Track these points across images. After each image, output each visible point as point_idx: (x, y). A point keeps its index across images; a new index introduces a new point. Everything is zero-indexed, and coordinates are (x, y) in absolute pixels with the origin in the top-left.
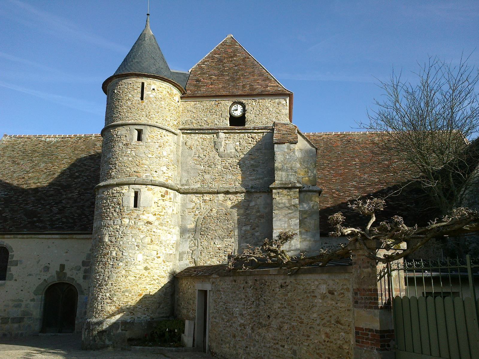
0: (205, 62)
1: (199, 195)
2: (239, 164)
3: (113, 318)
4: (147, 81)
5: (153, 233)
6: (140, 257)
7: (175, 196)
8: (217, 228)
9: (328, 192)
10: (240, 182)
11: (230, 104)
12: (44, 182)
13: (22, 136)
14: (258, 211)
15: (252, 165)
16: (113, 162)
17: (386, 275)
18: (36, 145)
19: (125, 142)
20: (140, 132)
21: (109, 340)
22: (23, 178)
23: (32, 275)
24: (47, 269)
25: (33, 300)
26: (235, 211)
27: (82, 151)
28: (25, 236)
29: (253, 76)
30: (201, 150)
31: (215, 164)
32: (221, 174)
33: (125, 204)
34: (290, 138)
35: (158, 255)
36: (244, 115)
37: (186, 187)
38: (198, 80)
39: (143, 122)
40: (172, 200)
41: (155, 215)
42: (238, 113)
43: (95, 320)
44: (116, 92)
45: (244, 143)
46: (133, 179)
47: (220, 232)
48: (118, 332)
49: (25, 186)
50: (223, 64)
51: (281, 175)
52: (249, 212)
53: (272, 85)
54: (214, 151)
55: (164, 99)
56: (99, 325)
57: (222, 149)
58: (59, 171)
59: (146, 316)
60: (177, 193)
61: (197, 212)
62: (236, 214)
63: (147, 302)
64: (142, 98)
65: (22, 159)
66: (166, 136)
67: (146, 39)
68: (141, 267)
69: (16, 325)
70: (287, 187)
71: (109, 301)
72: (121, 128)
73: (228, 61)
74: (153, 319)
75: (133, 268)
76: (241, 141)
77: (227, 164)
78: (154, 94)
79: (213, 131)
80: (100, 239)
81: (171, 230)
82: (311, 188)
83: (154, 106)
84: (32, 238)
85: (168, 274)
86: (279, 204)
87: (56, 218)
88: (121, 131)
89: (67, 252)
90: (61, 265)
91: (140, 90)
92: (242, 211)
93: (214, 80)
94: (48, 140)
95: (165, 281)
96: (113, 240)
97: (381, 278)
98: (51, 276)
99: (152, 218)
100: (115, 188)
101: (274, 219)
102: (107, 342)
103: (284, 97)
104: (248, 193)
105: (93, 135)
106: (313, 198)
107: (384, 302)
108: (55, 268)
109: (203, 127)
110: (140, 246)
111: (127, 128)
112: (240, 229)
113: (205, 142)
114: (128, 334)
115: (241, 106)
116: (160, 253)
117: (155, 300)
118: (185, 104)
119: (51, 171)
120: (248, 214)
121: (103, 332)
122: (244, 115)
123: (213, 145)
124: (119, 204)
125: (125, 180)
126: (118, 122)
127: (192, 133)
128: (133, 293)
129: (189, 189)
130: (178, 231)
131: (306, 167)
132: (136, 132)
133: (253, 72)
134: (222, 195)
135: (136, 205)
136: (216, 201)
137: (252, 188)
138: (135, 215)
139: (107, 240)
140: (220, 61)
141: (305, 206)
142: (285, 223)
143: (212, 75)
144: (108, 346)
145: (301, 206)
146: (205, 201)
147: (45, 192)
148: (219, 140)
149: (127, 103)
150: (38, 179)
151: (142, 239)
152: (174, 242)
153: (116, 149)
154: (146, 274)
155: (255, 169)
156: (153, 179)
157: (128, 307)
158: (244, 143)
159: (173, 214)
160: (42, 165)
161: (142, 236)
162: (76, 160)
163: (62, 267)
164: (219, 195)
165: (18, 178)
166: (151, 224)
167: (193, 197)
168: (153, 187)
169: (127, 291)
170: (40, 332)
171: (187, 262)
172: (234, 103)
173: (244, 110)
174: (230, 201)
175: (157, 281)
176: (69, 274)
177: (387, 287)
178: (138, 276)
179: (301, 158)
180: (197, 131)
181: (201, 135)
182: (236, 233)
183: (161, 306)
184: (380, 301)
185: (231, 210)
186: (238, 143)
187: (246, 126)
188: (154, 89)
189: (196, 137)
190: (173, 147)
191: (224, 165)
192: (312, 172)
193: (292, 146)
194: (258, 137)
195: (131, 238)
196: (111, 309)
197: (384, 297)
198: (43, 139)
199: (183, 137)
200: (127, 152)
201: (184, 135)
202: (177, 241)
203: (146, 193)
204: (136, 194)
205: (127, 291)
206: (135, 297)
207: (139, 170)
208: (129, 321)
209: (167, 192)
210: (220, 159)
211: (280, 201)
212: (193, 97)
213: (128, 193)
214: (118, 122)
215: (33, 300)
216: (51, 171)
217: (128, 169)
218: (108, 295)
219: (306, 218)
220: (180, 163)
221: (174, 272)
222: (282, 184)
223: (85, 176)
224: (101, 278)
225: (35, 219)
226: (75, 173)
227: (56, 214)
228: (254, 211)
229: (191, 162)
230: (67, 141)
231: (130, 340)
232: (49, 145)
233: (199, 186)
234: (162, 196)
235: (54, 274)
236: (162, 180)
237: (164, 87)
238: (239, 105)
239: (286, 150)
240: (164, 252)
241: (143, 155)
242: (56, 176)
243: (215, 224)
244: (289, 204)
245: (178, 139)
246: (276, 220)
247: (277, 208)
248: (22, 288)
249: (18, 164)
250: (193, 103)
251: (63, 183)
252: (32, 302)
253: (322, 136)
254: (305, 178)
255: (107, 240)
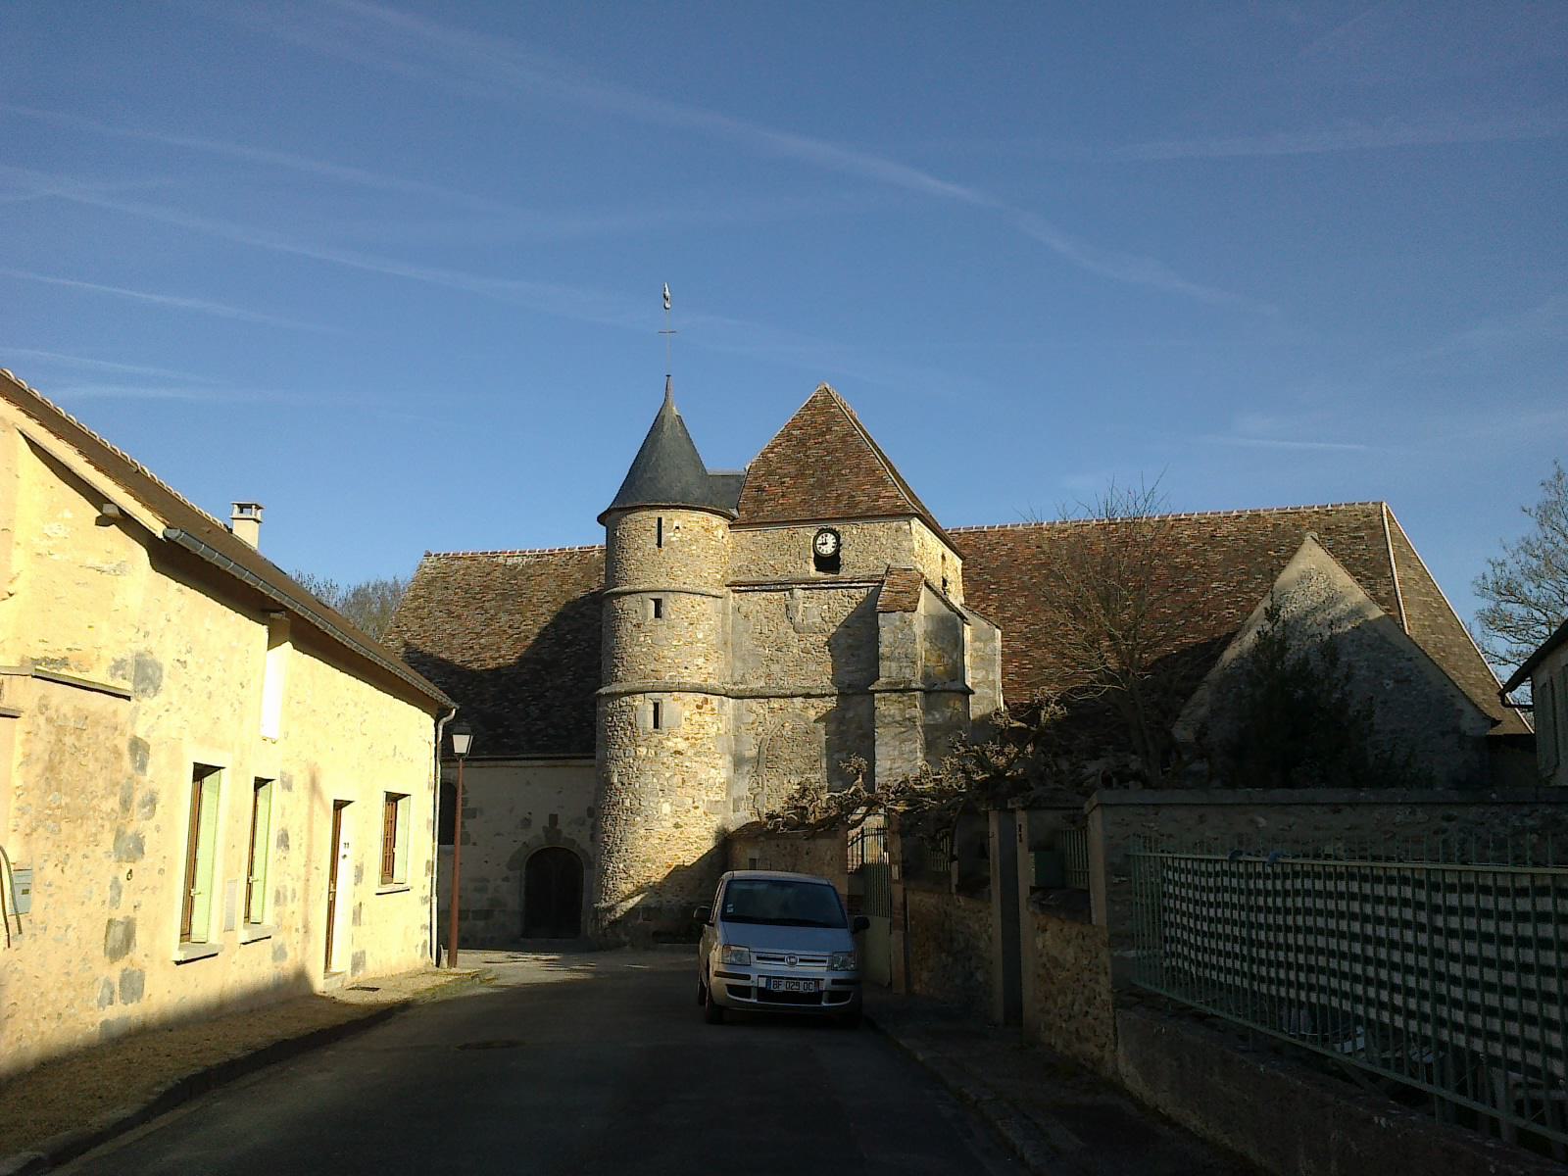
0: (775, 447)
1: (762, 700)
2: (827, 643)
3: (630, 901)
4: (665, 515)
5: (685, 769)
6: (666, 808)
7: (722, 704)
8: (792, 756)
9: (1053, 663)
10: (830, 677)
11: (815, 534)
12: (507, 654)
13: (461, 555)
14: (860, 728)
15: (850, 646)
16: (619, 655)
17: (860, 841)
18: (488, 574)
19: (634, 622)
20: (658, 603)
21: (626, 935)
22: (471, 648)
23: (502, 835)
24: (527, 823)
25: (506, 879)
26: (821, 726)
27: (576, 583)
28: (486, 764)
29: (857, 475)
30: (765, 620)
31: (788, 646)
32: (798, 663)
33: (640, 724)
34: (906, 602)
35: (696, 804)
36: (837, 551)
37: (742, 687)
38: (760, 489)
39: (661, 587)
40: (716, 712)
41: (688, 739)
42: (828, 549)
43: (604, 904)
44: (618, 534)
45: (835, 606)
46: (651, 682)
47: (798, 762)
48: (639, 922)
49: (475, 666)
50: (806, 451)
51: (890, 667)
52: (845, 728)
53: (887, 494)
54: (787, 622)
55: (697, 541)
56: (610, 912)
57: (798, 618)
58: (537, 631)
59: (678, 898)
60: (724, 698)
61: (760, 729)
62: (823, 732)
63: (681, 877)
64: (659, 544)
65: (464, 606)
66: (701, 604)
67: (665, 428)
68: (669, 824)
69: (481, 924)
70: (902, 689)
71: (624, 875)
72: (628, 597)
73: (816, 443)
74: (691, 904)
75: (655, 825)
76: (831, 602)
77: (808, 645)
78: (679, 535)
79: (783, 587)
80: (606, 778)
81: (717, 761)
82: (946, 687)
83: (680, 556)
84: (496, 767)
85: (714, 834)
86: (885, 717)
87: (537, 727)
88: (628, 602)
89: (560, 792)
90: (551, 815)
91: (655, 531)
92: (833, 727)
93: (788, 488)
94: (510, 562)
95: (708, 845)
96: (625, 780)
97: (852, 844)
98: (535, 835)
99: (682, 745)
100: (623, 699)
101: (877, 743)
102: (623, 937)
103: (907, 518)
104: (842, 695)
105: (597, 548)
106: (951, 703)
107: (855, 867)
108: (541, 822)
109: (768, 579)
110: (666, 791)
111: (638, 597)
112: (829, 757)
113: (771, 606)
114: (653, 926)
115: (833, 537)
116: (699, 800)
117: (692, 874)
118: (738, 537)
119: (520, 633)
120: (843, 731)
121: (614, 923)
122: (837, 551)
123: (784, 610)
124: (630, 724)
125: (637, 685)
126: (624, 588)
127: (748, 591)
128: (658, 864)
129: (745, 690)
130: (730, 762)
131: (940, 649)
132: (653, 603)
133: (858, 466)
134: (801, 699)
135: (656, 726)
136: (790, 710)
137: (849, 686)
138: (655, 741)
139: (616, 781)
140: (802, 443)
141: (937, 716)
142: (894, 750)
143: (785, 476)
144: (625, 944)
145: (930, 717)
146: (772, 710)
147: (513, 676)
148: (795, 602)
149: (636, 554)
150: (499, 649)
151: (668, 780)
152: (722, 780)
153: (622, 632)
154: (677, 835)
155: (856, 652)
156: (681, 680)
157: (651, 884)
158: (835, 606)
159: (718, 735)
160: (504, 618)
161: (667, 775)
162: (565, 605)
163: (554, 819)
164: (795, 700)
165: (462, 649)
166: (682, 754)
167: (753, 704)
168: (682, 694)
169: (648, 860)
170: (523, 936)
171: (747, 813)
172: (821, 532)
173: (838, 545)
174: (815, 709)
175: (695, 845)
176: (565, 832)
177: (860, 853)
178: (665, 837)
179: (931, 631)
180: (756, 588)
181: (764, 594)
182: (824, 765)
183: (703, 885)
184: (850, 867)
185: (815, 725)
186: (826, 607)
187: (841, 574)
188: (678, 528)
189: (756, 597)
190: (715, 621)
191: (803, 646)
192: (950, 658)
193: (907, 615)
194: (860, 595)
195: (651, 777)
196: (626, 887)
197: (855, 862)
198: (501, 560)
199: (734, 598)
200: (638, 638)
201: (736, 595)
202: (728, 779)
203: (671, 705)
204: (656, 705)
205: (648, 860)
206: (662, 870)
207: (659, 667)
208: (653, 906)
209: (706, 700)
210: (797, 636)
211: (886, 713)
212: (749, 524)
213: (644, 705)
214: (624, 588)
215: (506, 879)
216: (520, 633)
217: (642, 667)
218: (621, 866)
219: (939, 738)
220: (729, 645)
221: (725, 831)
222: (890, 683)
223: (584, 640)
224: (611, 841)
225: (500, 731)
226: (565, 635)
227: (536, 719)
228: (854, 726)
229: (749, 644)
230: (547, 564)
231: (656, 934)
232: (514, 573)
233: (762, 684)
234: (698, 707)
235: (541, 832)
236: (697, 680)
237: (695, 519)
238: (829, 535)
239: (898, 623)
240: (706, 799)
241: (665, 642)
242: (529, 642)
243: (790, 750)
244: (901, 716)
245: (725, 607)
246: (880, 745)
247: (881, 724)
248: (487, 859)
249: (459, 617)
250: (750, 534)
251: (545, 656)
252: (506, 883)
253: (1066, 531)
254: (937, 668)
255: (616, 781)
